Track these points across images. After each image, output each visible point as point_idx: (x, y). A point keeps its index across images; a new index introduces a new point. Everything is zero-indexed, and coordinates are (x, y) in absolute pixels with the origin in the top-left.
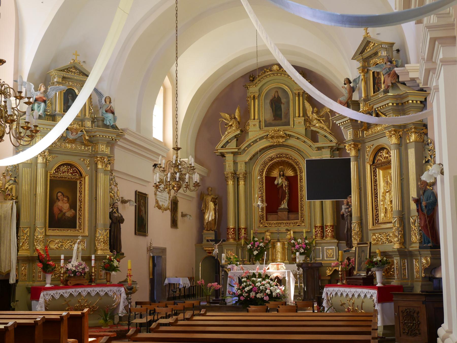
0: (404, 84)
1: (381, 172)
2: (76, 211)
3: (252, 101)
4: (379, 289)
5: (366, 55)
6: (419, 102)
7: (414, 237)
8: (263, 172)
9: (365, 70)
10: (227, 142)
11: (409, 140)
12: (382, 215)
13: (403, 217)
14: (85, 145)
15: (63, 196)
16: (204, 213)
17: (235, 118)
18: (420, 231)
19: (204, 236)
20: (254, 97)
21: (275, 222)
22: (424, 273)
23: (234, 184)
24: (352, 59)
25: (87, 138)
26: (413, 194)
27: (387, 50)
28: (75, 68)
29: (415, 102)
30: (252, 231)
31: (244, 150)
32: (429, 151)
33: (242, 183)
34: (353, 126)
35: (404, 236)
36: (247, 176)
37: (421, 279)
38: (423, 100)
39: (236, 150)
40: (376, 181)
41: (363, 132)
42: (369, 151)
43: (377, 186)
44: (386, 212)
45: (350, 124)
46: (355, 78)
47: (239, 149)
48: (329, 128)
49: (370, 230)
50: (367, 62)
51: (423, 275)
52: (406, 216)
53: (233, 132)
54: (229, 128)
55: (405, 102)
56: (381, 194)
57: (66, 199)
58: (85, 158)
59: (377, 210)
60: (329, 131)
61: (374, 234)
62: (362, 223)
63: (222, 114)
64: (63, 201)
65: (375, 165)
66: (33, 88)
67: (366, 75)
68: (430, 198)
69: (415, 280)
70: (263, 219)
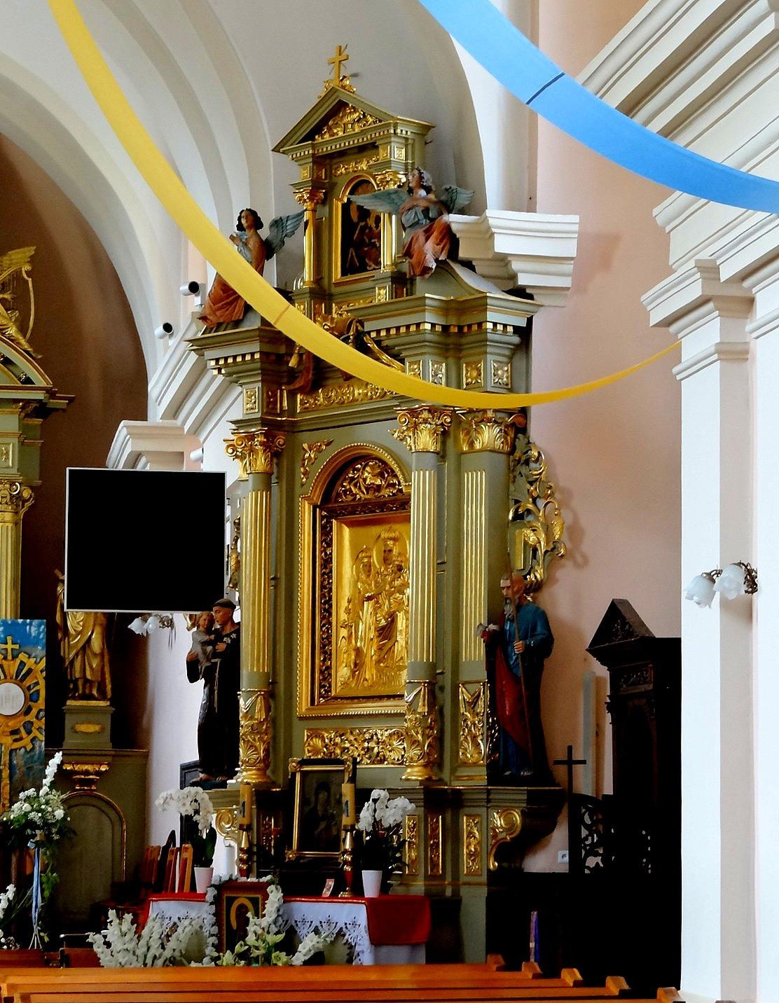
0: (468, 265)
1: (346, 531)
4: (372, 905)
5: (325, 143)
6: (510, 329)
7: (470, 747)
9: (320, 190)
11: (471, 444)
12: (342, 673)
13: (437, 686)
18: (489, 729)
19: (69, 721)
22: (495, 860)
24: (272, 150)
26: (475, 610)
27: (406, 146)
29: (500, 327)
32: (531, 483)
35: (438, 743)
37: (484, 879)
38: (523, 324)
40: (327, 562)
41: (292, 395)
42: (313, 463)
43: (330, 577)
44: (357, 666)
45: (259, 365)
46: (284, 215)
48: (22, 329)
49: (301, 718)
50: (325, 166)
51: (493, 865)
52: (447, 681)
55: (470, 326)
56: (344, 604)
59: (327, 655)
60: (26, 346)
61: (315, 734)
62: (275, 691)
65: (333, 507)
67: (319, 207)
68: (534, 629)
69: (463, 879)
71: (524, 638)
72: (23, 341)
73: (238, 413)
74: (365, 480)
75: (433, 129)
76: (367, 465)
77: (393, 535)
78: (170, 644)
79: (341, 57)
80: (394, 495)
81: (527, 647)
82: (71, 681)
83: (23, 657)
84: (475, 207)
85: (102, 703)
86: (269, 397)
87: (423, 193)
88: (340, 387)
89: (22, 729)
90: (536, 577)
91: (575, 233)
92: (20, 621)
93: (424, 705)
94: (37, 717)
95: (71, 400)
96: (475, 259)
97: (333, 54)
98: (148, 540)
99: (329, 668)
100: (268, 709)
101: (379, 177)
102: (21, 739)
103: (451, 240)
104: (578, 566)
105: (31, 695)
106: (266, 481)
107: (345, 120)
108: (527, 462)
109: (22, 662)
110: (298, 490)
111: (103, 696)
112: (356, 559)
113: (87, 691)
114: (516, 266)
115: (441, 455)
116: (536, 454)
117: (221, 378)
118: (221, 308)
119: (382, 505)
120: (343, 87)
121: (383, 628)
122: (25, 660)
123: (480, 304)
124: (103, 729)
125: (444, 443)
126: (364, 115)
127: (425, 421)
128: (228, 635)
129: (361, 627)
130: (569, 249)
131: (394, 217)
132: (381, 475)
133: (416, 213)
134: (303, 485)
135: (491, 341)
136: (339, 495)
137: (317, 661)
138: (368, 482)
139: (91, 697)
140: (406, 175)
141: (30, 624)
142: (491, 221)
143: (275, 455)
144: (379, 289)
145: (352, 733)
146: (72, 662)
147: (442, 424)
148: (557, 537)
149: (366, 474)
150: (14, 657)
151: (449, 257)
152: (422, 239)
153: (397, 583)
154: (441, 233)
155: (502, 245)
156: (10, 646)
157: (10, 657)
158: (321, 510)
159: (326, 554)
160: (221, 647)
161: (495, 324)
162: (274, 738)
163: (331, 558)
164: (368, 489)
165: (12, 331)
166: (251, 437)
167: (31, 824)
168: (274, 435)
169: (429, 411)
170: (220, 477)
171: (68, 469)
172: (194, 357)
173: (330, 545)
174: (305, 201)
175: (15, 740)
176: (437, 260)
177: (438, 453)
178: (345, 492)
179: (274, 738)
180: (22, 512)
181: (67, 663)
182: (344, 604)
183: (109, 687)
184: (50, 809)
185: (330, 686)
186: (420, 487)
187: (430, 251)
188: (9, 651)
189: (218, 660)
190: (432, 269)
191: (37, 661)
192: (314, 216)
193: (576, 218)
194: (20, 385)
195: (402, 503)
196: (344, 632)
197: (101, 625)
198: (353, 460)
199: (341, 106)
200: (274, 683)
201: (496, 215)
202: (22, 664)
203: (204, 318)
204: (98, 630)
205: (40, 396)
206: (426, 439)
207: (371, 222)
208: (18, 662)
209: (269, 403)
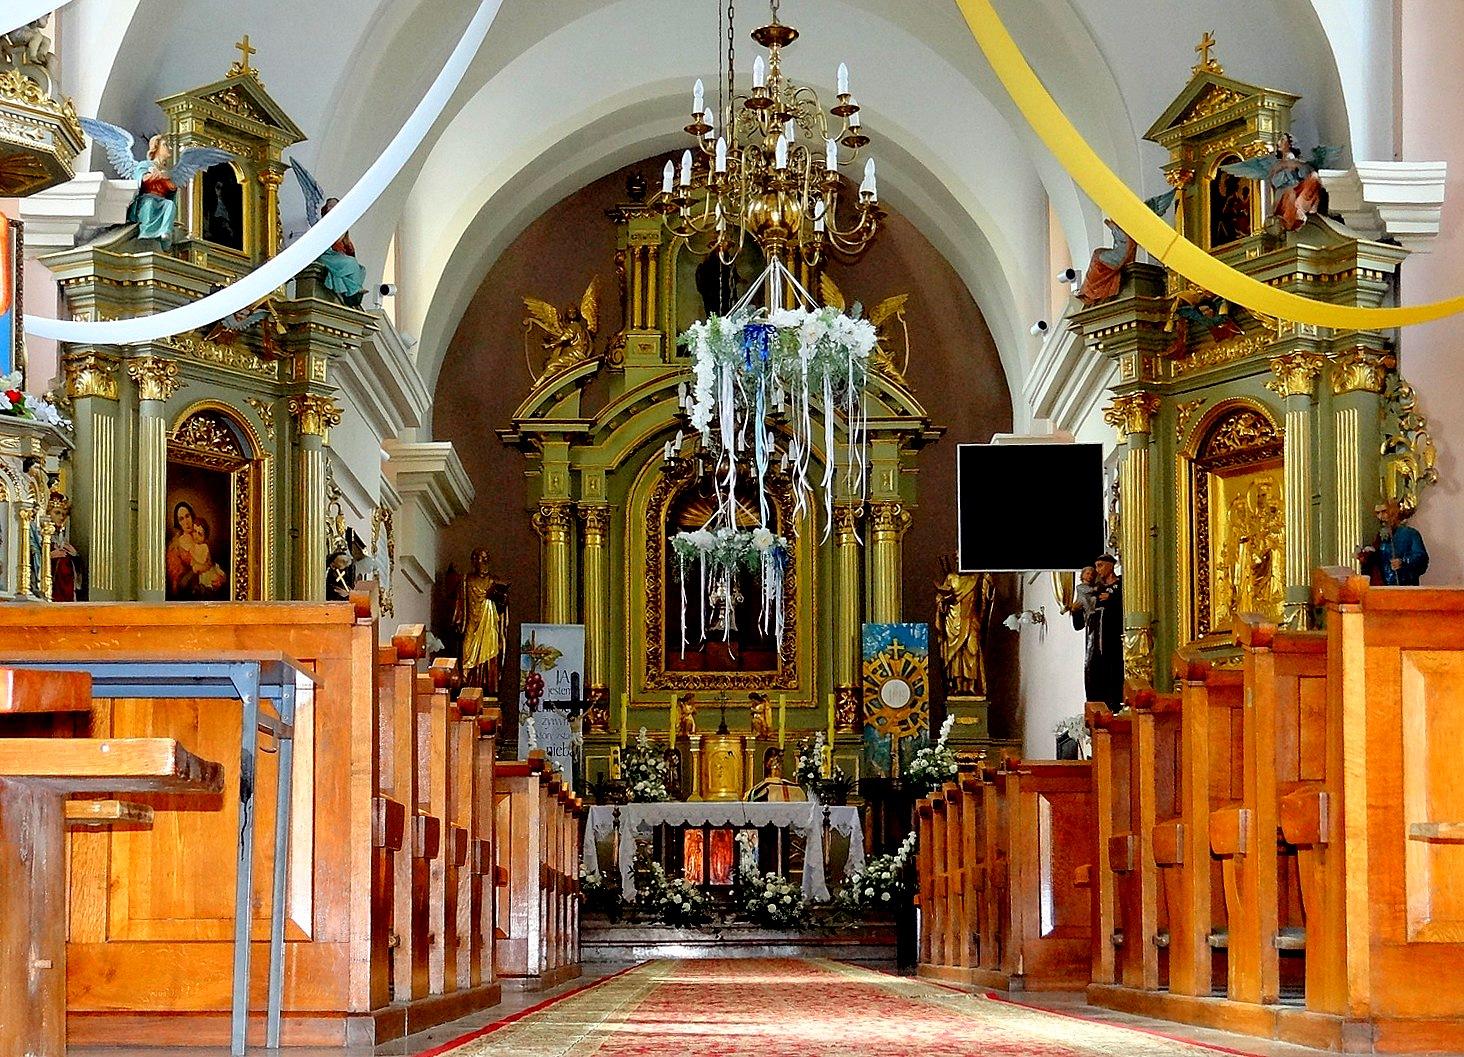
0: (1339, 219)
1: (1221, 482)
2: (226, 568)
3: (638, 265)
5: (1195, 125)
6: (1379, 275)
8: (659, 506)
10: (553, 399)
11: (1343, 385)
14: (265, 356)
15: (194, 517)
16: (462, 638)
17: (579, 318)
20: (645, 249)
21: (697, 675)
23: (568, 543)
25: (282, 330)
27: (1273, 118)
28: (239, 91)
29: (1369, 273)
30: (625, 698)
31: (607, 430)
33: (594, 540)
34: (1140, 340)
36: (612, 522)
39: (584, 428)
40: (1204, 510)
43: (1207, 525)
44: (1234, 603)
47: (593, 424)
53: (576, 363)
54: (558, 351)
56: (1220, 548)
57: (199, 529)
58: (261, 398)
59: (1205, 594)
60: (902, 382)
63: (532, 304)
64: (191, 533)
65: (1206, 461)
66: (128, 149)
68: (1409, 547)
70: (657, 665)
71: (1399, 556)
72: (899, 378)
73: (1116, 382)
74: (1238, 432)
75: (1298, 102)
76: (1240, 418)
77: (1266, 481)
78: (1042, 638)
79: (1208, 43)
80: (1267, 442)
81: (1403, 564)
82: (950, 680)
83: (907, 656)
84: (1344, 161)
85: (979, 698)
86: (1145, 364)
87: (1291, 156)
88: (1212, 349)
89: (909, 720)
90: (1409, 504)
91: (1443, 178)
92: (904, 625)
93: (1303, 625)
94: (922, 709)
95: (943, 431)
96: (1345, 212)
97: (1200, 41)
98: (1039, 505)
99: (1208, 607)
100: (1151, 647)
101: (1248, 149)
102: (909, 728)
103: (1321, 195)
104: (1450, 492)
105: (916, 690)
106: (1145, 439)
107: (1213, 103)
108: (1397, 399)
109: (907, 660)
110: (1174, 445)
111: (979, 692)
112: (1231, 505)
113: (965, 689)
114: (1384, 214)
115: (1314, 399)
116: (1407, 390)
117: (1099, 354)
118: (1098, 286)
119: (1255, 452)
120: (1211, 70)
121: (1259, 565)
122: (910, 659)
123: (1350, 251)
124: (980, 721)
125: (1316, 388)
126: (1231, 95)
127: (1299, 365)
128: (1111, 586)
129: (1238, 566)
130: (1437, 194)
131: (1262, 182)
132: (1254, 426)
133: (1286, 175)
134: (1178, 442)
135: (1362, 288)
136: (1213, 449)
137: (1196, 601)
138: (1241, 433)
139: (969, 693)
140: (1273, 145)
141: (914, 628)
142: (1360, 172)
143: (1151, 416)
144: (1250, 251)
145: (1232, 662)
146: (950, 663)
147: (1314, 368)
148: (1430, 464)
149: (1239, 426)
150: (900, 657)
151: (1319, 211)
152: (1293, 195)
153: (1272, 523)
154: (1310, 189)
155: (1371, 194)
156: (896, 647)
157: (896, 657)
158: (1196, 464)
159: (1202, 504)
160: (1104, 596)
161: (1365, 270)
162: (1158, 670)
163: (1207, 508)
164: (1241, 440)
165: (890, 368)
166: (1130, 400)
167: (930, 778)
168: (1149, 402)
169: (1302, 356)
170: (1097, 449)
171: (958, 446)
172: (1073, 336)
173: (1205, 495)
174: (1176, 181)
175: (903, 730)
176: (1307, 214)
177: (1310, 395)
178: (1219, 445)
179: (1158, 670)
180: (902, 532)
181: (947, 663)
182: (1220, 548)
183: (984, 685)
184: (945, 764)
185: (1208, 623)
186: (1294, 434)
187: (1301, 206)
188: (896, 651)
189: (1102, 609)
190: (1118, 708)
191: (921, 661)
192: (1184, 194)
193: (1444, 165)
194: (896, 416)
195: (1276, 447)
196: (1220, 574)
197: (976, 630)
198: (1229, 412)
199: (1209, 88)
200: (1156, 621)
201: (1364, 165)
202: (908, 663)
203: (1081, 297)
204: (974, 633)
205: (917, 425)
206: (1299, 383)
207: (1239, 195)
208: (904, 660)
209: (1145, 369)
